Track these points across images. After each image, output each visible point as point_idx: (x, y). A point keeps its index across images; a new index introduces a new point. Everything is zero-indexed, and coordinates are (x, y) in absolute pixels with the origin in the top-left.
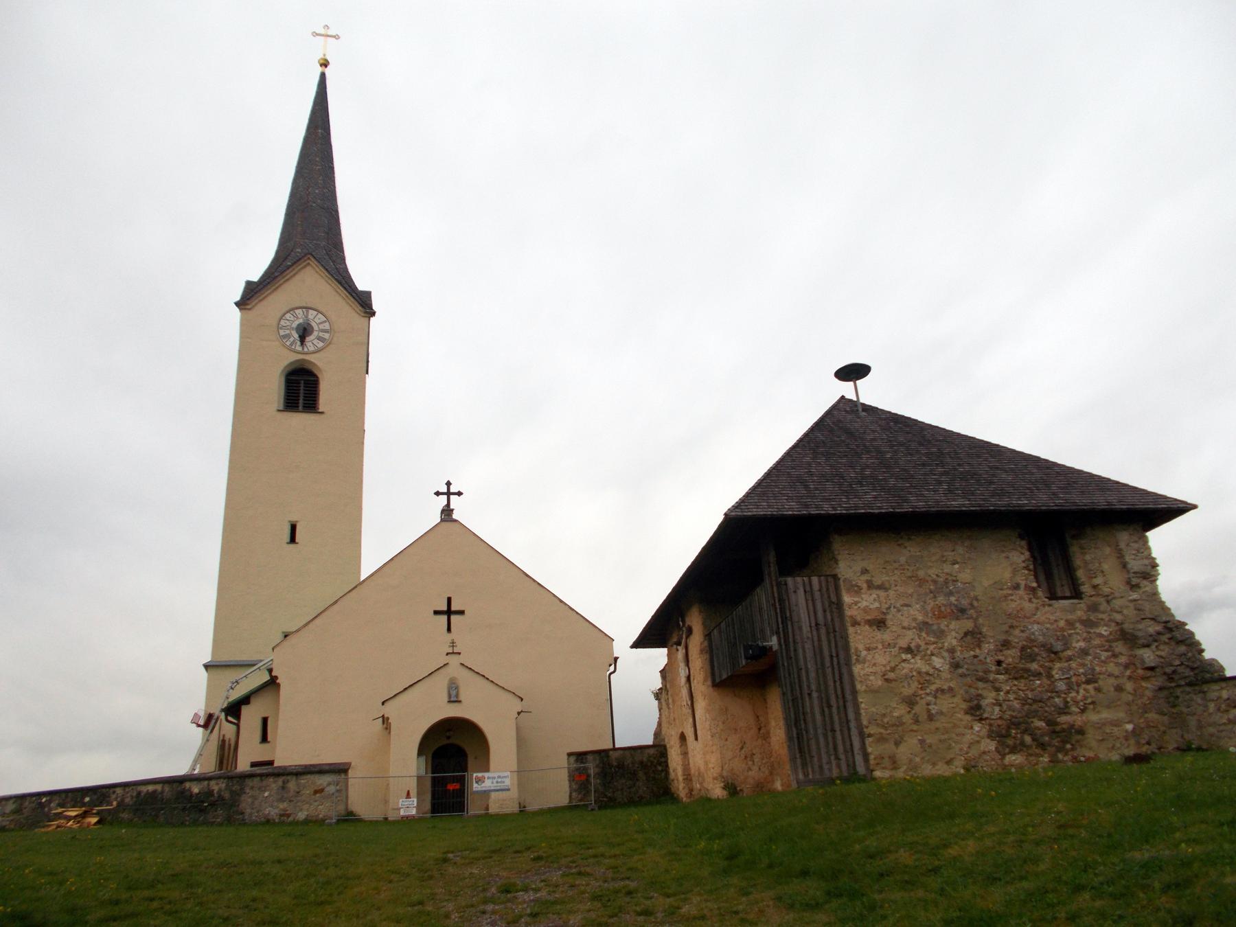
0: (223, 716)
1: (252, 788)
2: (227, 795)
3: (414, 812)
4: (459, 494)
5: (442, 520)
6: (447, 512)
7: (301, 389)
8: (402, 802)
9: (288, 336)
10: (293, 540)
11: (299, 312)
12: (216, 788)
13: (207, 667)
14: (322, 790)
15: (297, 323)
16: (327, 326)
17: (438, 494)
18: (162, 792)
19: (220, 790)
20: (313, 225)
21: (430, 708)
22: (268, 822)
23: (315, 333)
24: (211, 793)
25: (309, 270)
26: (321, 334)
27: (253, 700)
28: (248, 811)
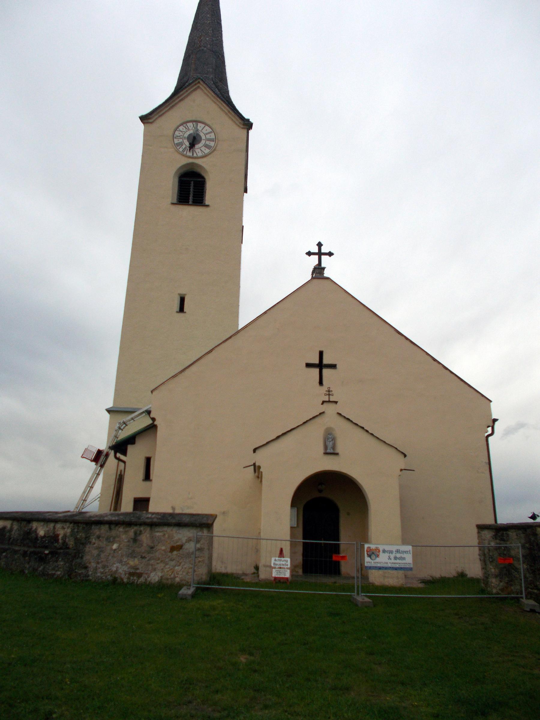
0: (112, 453)
1: (98, 537)
2: (71, 543)
3: (287, 575)
4: (330, 254)
5: (313, 278)
6: (318, 270)
7: (191, 188)
8: (275, 561)
9: (181, 144)
10: (182, 309)
11: (190, 125)
12: (61, 533)
13: (109, 411)
14: (180, 547)
15: (188, 133)
16: (212, 136)
17: (309, 254)
18: (11, 530)
19: (65, 536)
20: (204, 61)
21: (303, 460)
22: (115, 582)
23: (203, 142)
24: (55, 538)
25: (199, 92)
26: (208, 143)
27: (137, 440)
28: (93, 565)
